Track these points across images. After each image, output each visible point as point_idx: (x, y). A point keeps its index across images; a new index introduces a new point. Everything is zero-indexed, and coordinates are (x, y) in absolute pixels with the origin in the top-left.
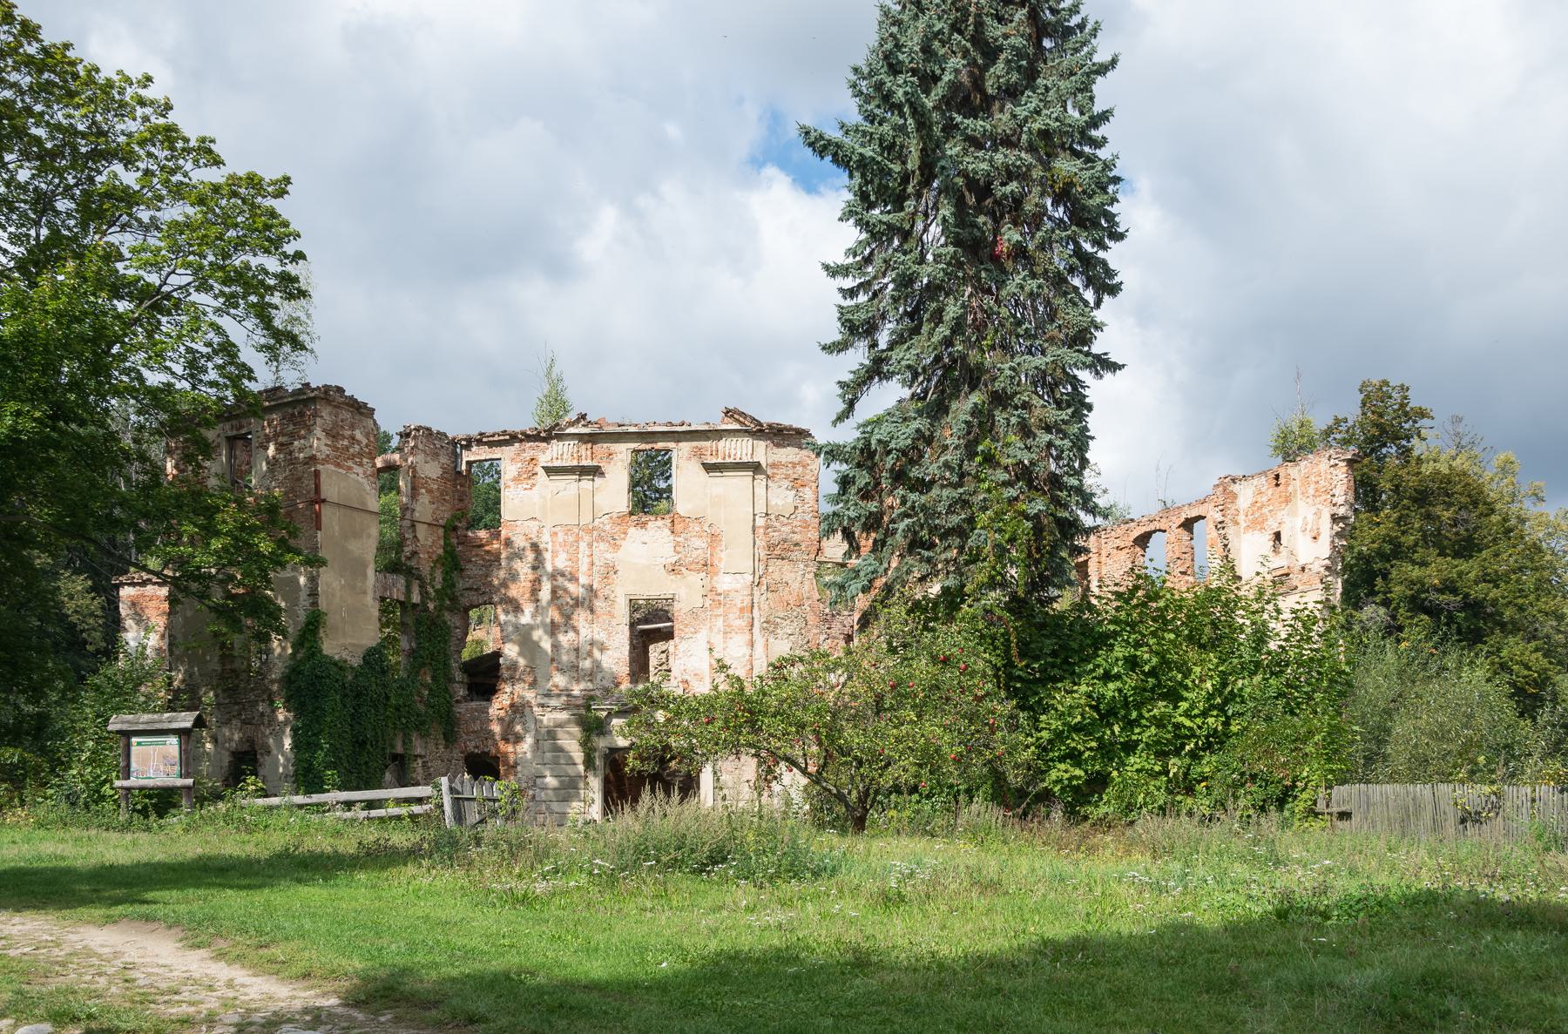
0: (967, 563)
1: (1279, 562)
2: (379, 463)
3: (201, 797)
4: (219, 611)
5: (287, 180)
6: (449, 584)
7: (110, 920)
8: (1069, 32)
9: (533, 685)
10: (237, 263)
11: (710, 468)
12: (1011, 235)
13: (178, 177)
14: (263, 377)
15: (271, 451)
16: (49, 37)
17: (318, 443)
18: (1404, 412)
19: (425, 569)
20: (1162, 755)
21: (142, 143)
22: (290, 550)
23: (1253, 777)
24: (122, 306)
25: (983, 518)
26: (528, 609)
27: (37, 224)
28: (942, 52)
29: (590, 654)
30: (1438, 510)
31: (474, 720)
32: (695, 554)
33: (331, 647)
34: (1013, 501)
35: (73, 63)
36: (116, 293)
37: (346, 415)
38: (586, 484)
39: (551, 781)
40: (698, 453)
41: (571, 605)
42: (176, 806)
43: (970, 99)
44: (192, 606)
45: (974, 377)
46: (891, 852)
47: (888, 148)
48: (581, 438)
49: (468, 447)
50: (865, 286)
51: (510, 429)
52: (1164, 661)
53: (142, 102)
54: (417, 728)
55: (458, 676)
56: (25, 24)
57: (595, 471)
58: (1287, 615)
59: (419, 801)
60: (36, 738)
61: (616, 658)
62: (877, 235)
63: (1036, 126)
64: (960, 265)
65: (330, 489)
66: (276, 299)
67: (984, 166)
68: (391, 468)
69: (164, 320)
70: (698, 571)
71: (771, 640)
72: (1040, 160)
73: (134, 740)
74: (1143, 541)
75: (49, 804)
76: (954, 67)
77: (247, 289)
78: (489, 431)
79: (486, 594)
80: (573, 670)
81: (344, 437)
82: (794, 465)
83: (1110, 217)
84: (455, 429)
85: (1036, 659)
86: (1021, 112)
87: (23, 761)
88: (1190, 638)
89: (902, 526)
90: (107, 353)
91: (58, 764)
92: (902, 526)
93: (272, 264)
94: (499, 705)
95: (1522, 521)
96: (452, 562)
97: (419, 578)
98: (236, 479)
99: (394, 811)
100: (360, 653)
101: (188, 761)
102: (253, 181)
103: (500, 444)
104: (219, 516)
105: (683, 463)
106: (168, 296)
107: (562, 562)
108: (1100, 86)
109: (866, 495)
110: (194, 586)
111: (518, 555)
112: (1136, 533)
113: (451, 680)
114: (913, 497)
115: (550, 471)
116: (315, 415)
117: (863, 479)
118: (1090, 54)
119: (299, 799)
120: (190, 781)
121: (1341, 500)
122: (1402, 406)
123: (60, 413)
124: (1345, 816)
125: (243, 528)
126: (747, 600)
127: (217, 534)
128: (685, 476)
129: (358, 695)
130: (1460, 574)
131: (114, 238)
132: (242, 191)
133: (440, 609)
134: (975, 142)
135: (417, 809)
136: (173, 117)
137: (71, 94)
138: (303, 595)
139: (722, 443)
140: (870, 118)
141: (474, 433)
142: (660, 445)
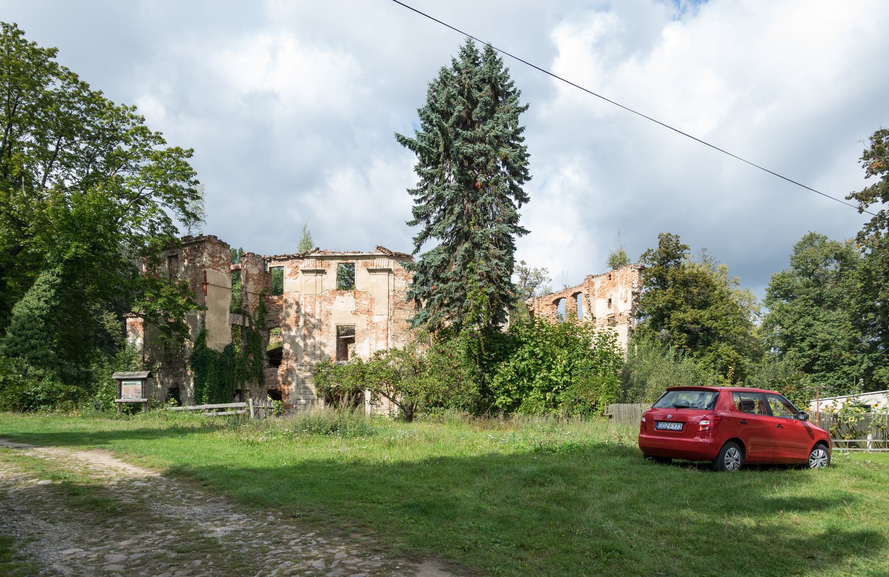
0: (464, 312)
1: (611, 311)
2: (232, 267)
3: (151, 406)
4: (162, 328)
5: (192, 150)
6: (262, 319)
7: (90, 449)
8: (509, 94)
9: (296, 361)
10: (172, 185)
11: (370, 271)
12: (481, 179)
13: (147, 148)
14: (182, 231)
15: (186, 263)
16: (92, 89)
17: (205, 259)
18: (677, 247)
19: (251, 312)
20: (544, 392)
21: (132, 134)
22: (192, 303)
23: (580, 401)
24: (124, 201)
25: (469, 294)
26: (294, 329)
27: (88, 167)
28: (454, 103)
29: (320, 348)
30: (691, 289)
31: (271, 375)
33: (210, 344)
34: (481, 287)
35: (104, 101)
36: (121, 195)
37: (218, 248)
38: (319, 277)
39: (303, 401)
40: (366, 265)
41: (311, 328)
42: (140, 410)
43: (466, 123)
44: (152, 328)
45: (467, 236)
46: (420, 427)
47: (433, 143)
48: (317, 258)
49: (270, 261)
50: (424, 198)
51: (288, 254)
52: (546, 354)
53: (132, 118)
54: (247, 379)
55: (265, 357)
56: (83, 84)
57: (322, 272)
58: (597, 335)
59: (241, 408)
60: (86, 382)
61: (331, 349)
62: (429, 178)
63: (492, 134)
64: (461, 191)
65: (210, 279)
66: (188, 200)
67: (470, 150)
68: (238, 270)
69: (141, 207)
72: (493, 148)
73: (123, 383)
74: (557, 302)
75: (87, 409)
76: (459, 109)
77: (177, 197)
78: (279, 255)
79: (277, 323)
80: (313, 355)
83: (526, 171)
84: (266, 253)
85: (493, 352)
86: (486, 128)
87: (77, 390)
88: (556, 344)
89: (436, 297)
90: (116, 221)
91: (92, 393)
92: (436, 297)
93: (185, 185)
94: (281, 370)
95: (729, 294)
96: (263, 309)
97: (249, 316)
98: (172, 274)
99: (229, 412)
100: (223, 347)
101: (145, 392)
102: (178, 150)
103: (283, 260)
104: (162, 290)
105: (359, 269)
106: (143, 197)
107: (308, 310)
108: (521, 117)
109: (423, 284)
110: (152, 319)
111: (290, 306)
112: (554, 298)
113: (262, 359)
114: (441, 285)
115: (304, 271)
116: (204, 248)
117: (422, 278)
118: (517, 104)
119: (191, 407)
120: (146, 400)
121: (636, 286)
122: (677, 244)
123: (95, 247)
124: (611, 417)
125: (172, 294)
126: (385, 327)
127: (161, 297)
128: (361, 275)
129: (222, 365)
130: (701, 316)
131: (121, 173)
132: (173, 155)
133: (257, 329)
134: (466, 140)
135: (239, 412)
136: (145, 124)
137: (102, 114)
138: (199, 323)
140: (426, 129)
141: (272, 255)
142: (350, 261)
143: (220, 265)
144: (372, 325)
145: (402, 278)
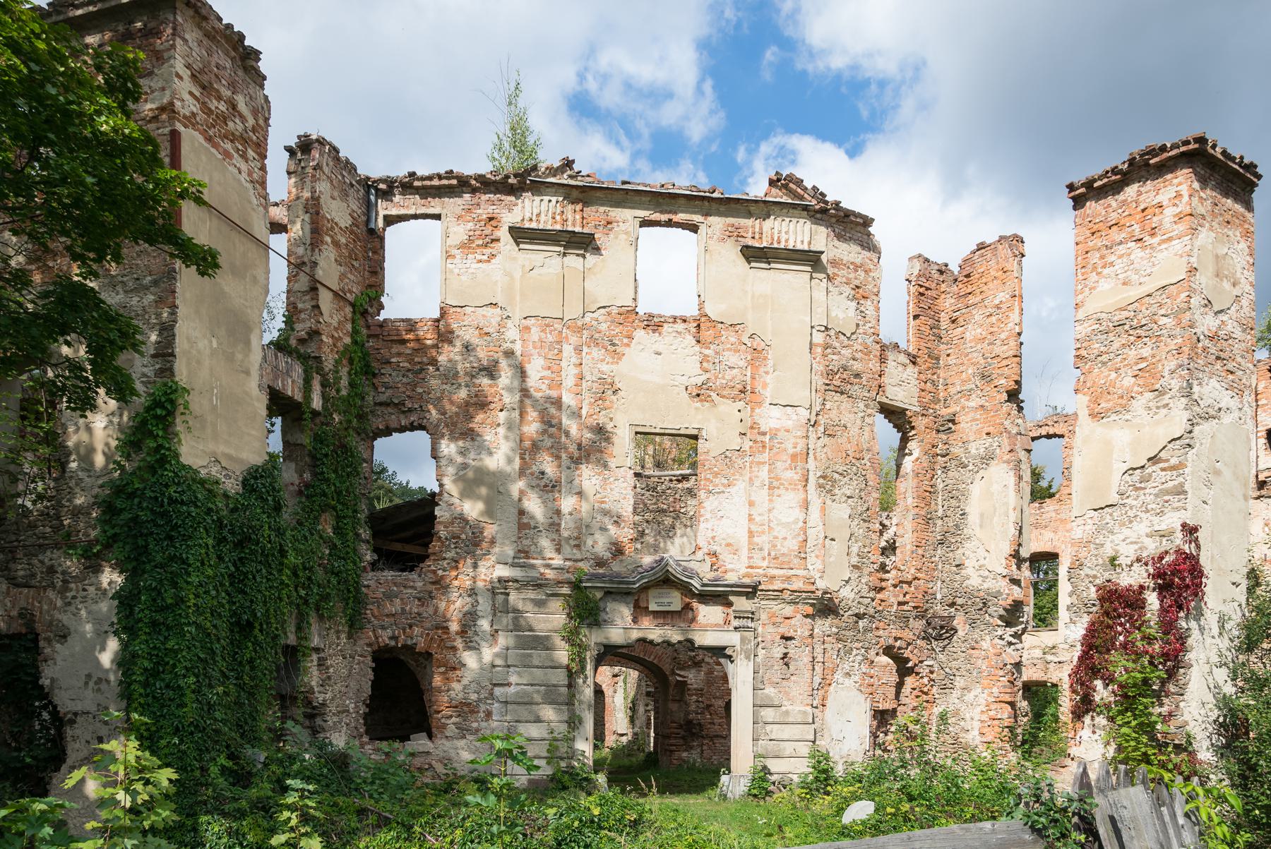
11: (753, 255)
32: (729, 374)
49: (387, 195)
70: (734, 399)
71: (829, 502)
81: (219, 98)
82: (857, 267)
100: (239, 470)
115: (521, 235)
139: (768, 224)
141: (400, 172)
143: (231, 137)
144: (756, 436)
145: (848, 290)
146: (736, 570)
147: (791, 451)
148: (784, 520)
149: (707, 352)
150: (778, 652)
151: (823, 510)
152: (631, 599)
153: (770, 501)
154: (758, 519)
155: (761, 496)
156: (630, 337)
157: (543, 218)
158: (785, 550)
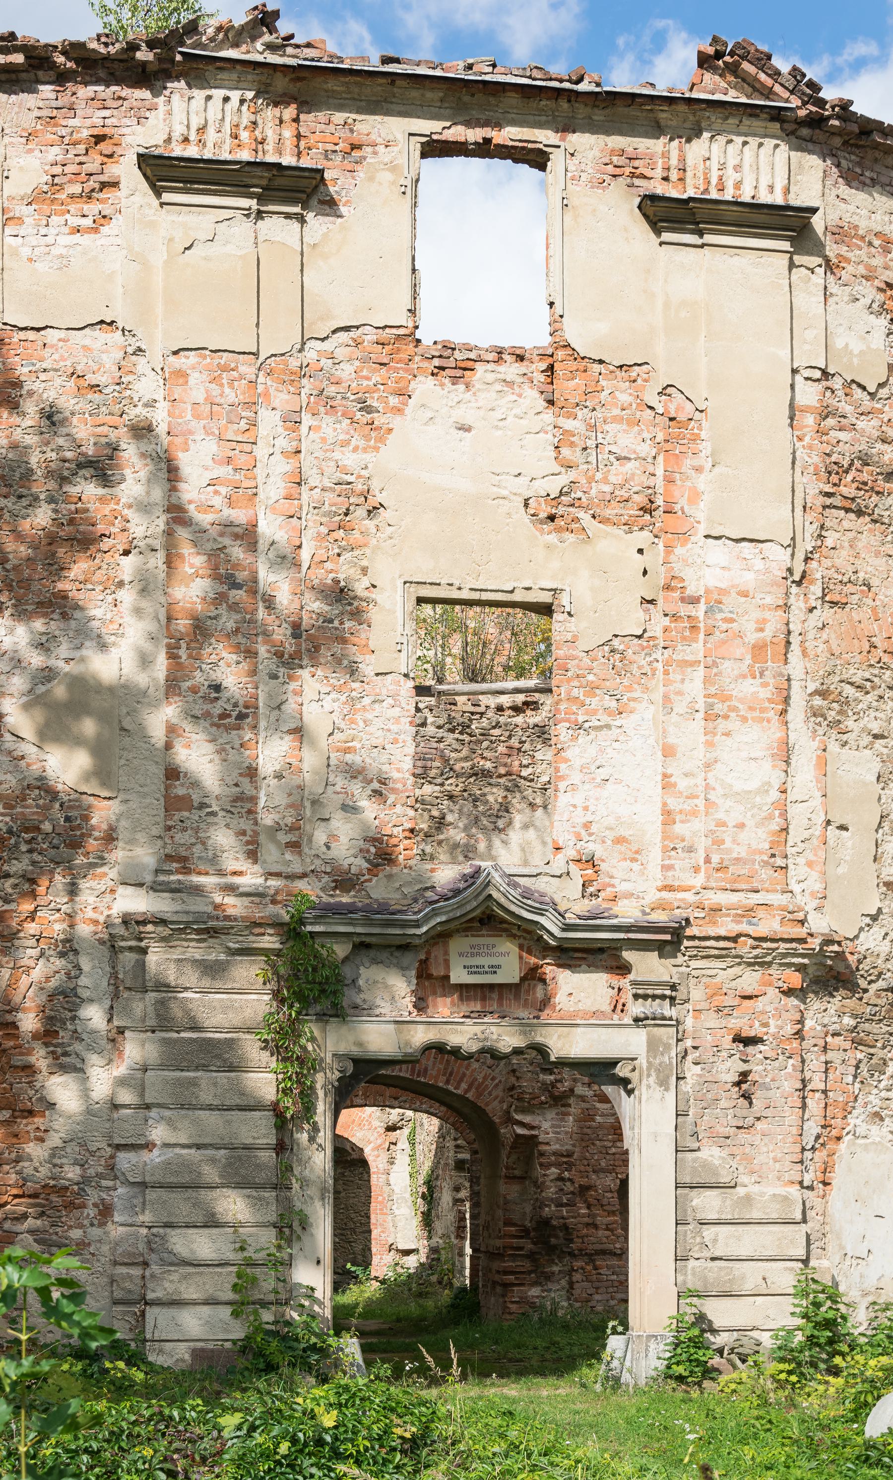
32: (618, 472)
38: (278, 229)
126: (774, 624)
146: (636, 895)
147: (752, 637)
148: (738, 786)
149: (569, 424)
150: (728, 1069)
151: (822, 764)
152: (411, 959)
153: (709, 744)
154: (683, 784)
155: (690, 734)
156: (404, 394)
157: (211, 136)
158: (740, 851)
